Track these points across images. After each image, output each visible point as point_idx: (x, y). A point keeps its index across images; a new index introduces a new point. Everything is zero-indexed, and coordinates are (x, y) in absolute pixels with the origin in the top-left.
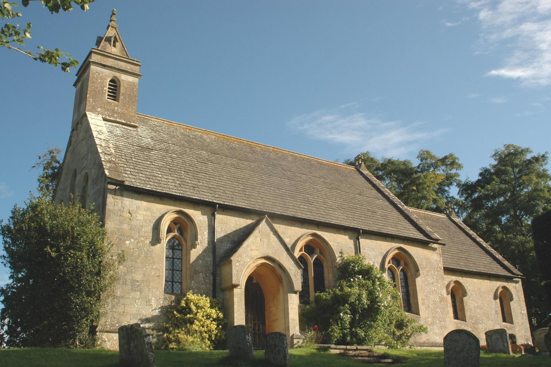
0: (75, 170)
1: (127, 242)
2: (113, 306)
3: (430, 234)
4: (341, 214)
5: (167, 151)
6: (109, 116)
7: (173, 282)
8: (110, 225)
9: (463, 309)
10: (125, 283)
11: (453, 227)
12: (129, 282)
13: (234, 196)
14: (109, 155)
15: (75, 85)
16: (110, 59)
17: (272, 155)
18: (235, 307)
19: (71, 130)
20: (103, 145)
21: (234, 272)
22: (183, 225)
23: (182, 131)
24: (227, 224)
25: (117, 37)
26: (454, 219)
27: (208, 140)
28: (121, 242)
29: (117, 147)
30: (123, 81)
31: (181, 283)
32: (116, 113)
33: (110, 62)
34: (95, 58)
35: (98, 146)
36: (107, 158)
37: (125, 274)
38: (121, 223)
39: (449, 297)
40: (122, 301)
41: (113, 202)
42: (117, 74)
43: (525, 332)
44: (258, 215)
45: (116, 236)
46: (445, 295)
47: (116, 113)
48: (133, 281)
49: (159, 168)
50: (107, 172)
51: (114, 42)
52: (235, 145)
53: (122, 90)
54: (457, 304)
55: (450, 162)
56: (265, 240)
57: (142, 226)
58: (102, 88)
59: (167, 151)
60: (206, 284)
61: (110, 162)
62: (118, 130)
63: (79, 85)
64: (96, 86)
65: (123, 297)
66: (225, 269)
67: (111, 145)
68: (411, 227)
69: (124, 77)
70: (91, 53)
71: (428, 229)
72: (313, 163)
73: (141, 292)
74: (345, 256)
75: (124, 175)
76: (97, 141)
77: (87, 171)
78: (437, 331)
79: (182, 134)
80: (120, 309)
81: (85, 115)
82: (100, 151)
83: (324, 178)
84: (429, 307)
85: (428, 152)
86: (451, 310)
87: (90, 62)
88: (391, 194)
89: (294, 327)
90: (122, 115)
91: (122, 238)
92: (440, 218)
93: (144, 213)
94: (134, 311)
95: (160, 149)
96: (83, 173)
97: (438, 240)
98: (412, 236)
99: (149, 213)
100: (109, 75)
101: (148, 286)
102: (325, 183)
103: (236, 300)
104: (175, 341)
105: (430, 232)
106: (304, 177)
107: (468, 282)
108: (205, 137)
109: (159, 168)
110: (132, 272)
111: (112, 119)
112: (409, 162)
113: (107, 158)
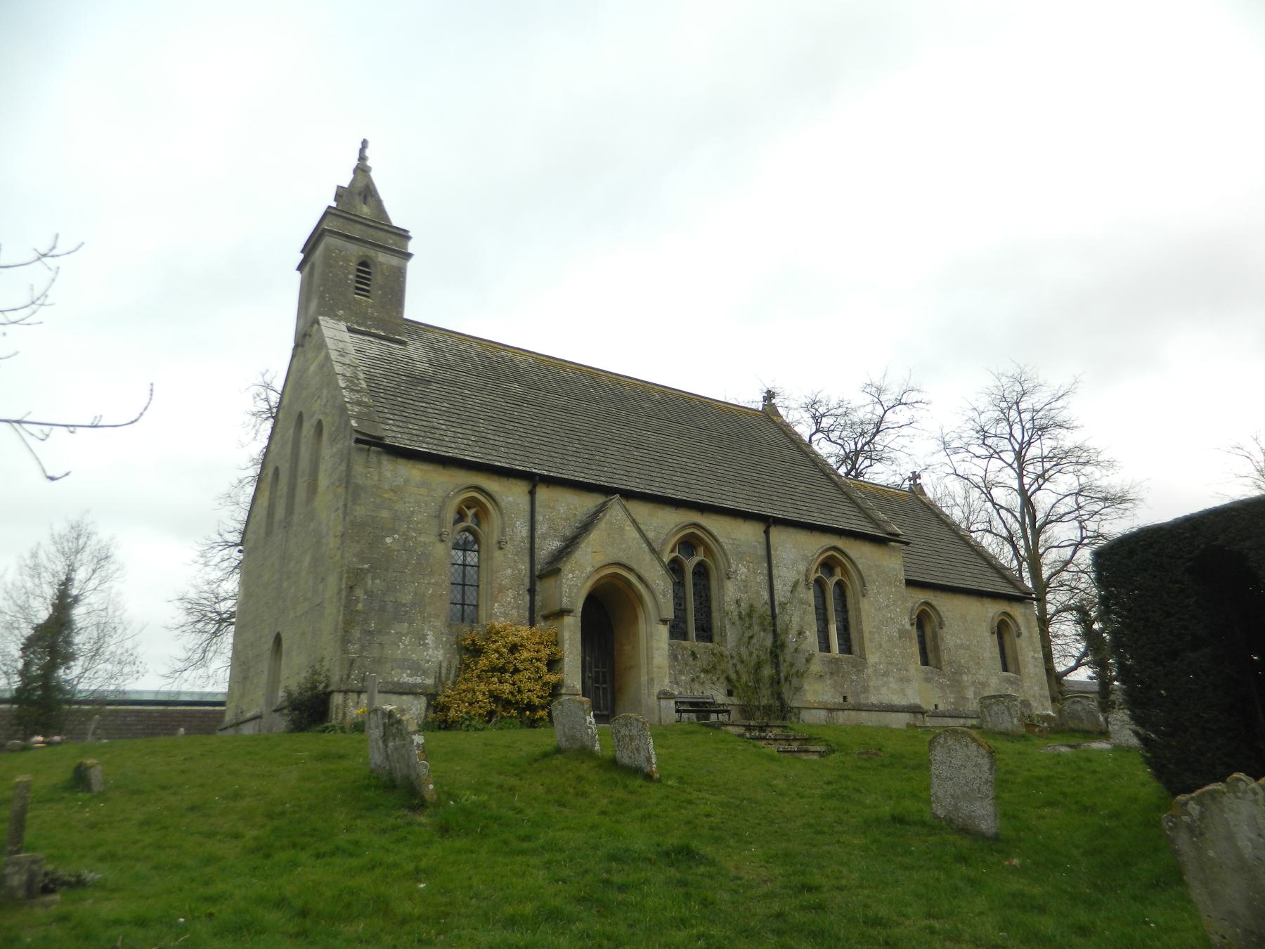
1: (388, 540)
3: (884, 524)
6: (359, 324)
9: (936, 648)
14: (357, 391)
15: (300, 268)
19: (292, 345)
24: (564, 508)
30: (381, 264)
31: (477, 606)
32: (371, 318)
39: (914, 631)
42: (371, 252)
43: (1041, 688)
44: (607, 491)
46: (908, 627)
47: (371, 318)
50: (1242, 775)
54: (928, 640)
57: (413, 512)
58: (346, 275)
60: (518, 608)
61: (359, 403)
62: (374, 348)
63: (307, 269)
65: (379, 632)
67: (362, 376)
73: (410, 623)
78: (893, 686)
79: (479, 354)
84: (881, 646)
86: (916, 649)
96: (314, 421)
97: (898, 535)
98: (853, 528)
107: (947, 606)
113: (356, 396)
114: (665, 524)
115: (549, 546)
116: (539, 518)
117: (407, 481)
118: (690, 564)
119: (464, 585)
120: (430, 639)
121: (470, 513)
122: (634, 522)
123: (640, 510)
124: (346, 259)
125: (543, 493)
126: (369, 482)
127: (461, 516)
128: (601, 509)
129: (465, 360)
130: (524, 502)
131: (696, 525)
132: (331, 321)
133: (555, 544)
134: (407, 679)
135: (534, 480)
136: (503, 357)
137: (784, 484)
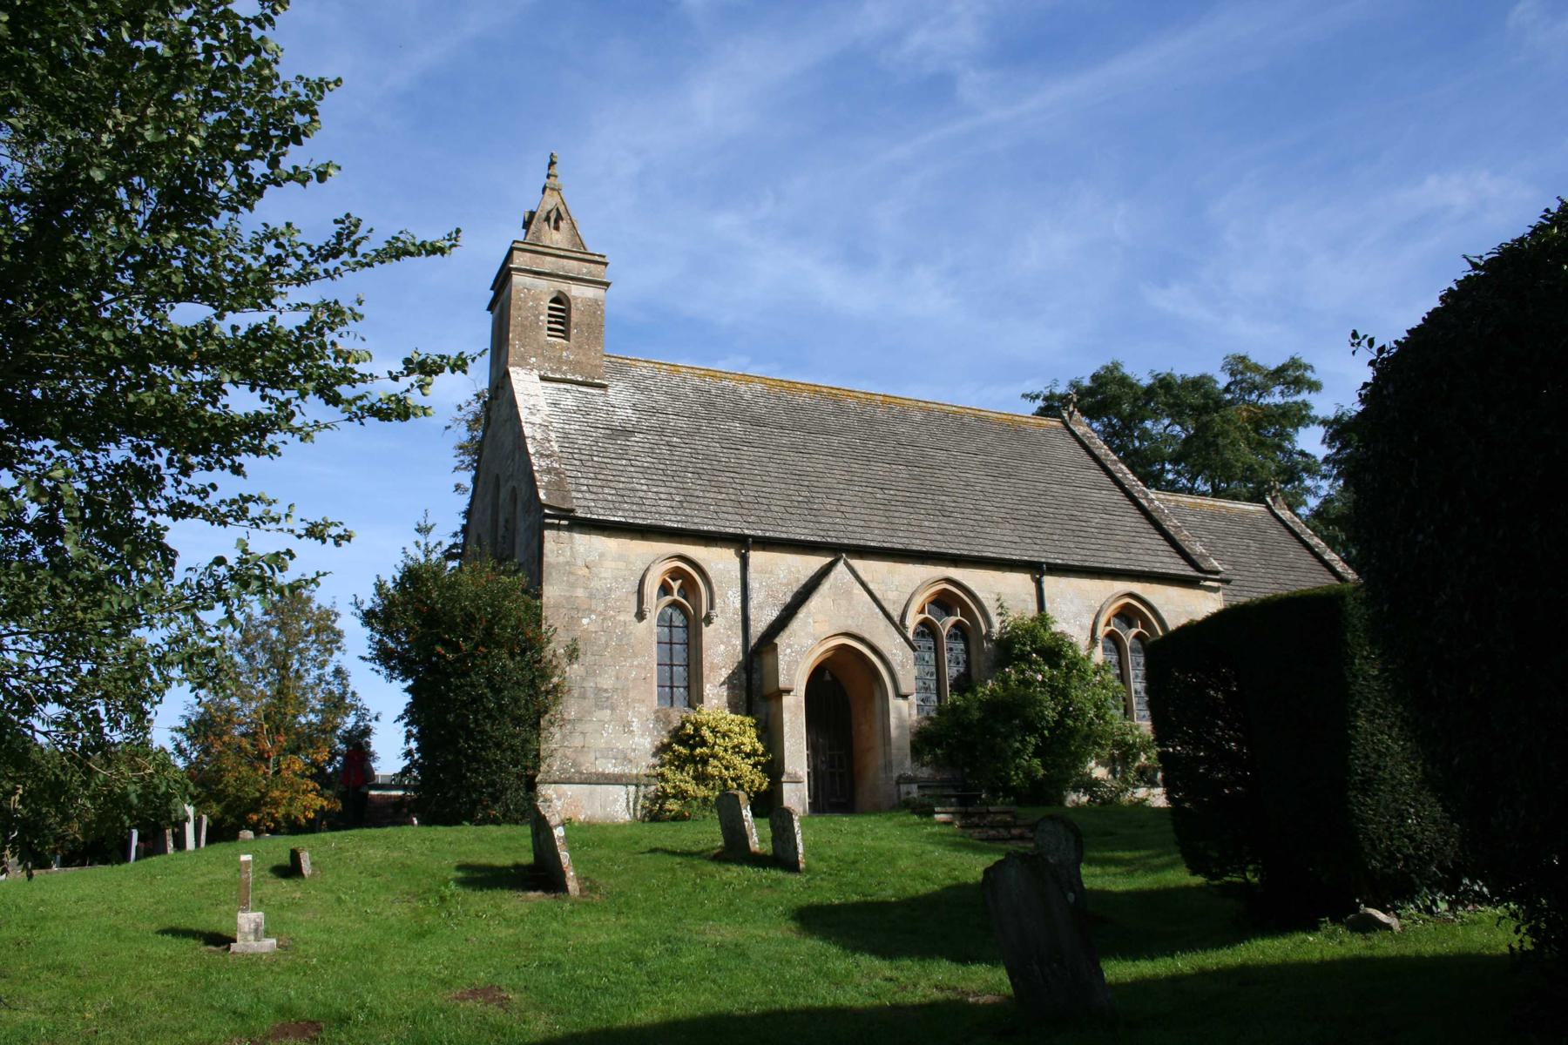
0: (497, 477)
1: (585, 621)
2: (564, 737)
4: (1007, 532)
5: (661, 432)
6: (552, 370)
7: (671, 687)
8: (552, 592)
10: (583, 696)
11: (1275, 532)
12: (590, 694)
13: (787, 516)
14: (548, 456)
15: (490, 308)
16: (548, 258)
17: (880, 414)
18: (786, 729)
20: (538, 437)
21: (782, 666)
22: (687, 586)
23: (697, 381)
24: (779, 572)
25: (562, 209)
26: (1279, 512)
27: (748, 396)
28: (574, 621)
29: (565, 436)
30: (576, 298)
32: (566, 362)
33: (548, 264)
34: (520, 260)
35: (529, 441)
36: (544, 463)
37: (583, 679)
38: (572, 586)
40: (579, 728)
41: (559, 547)
42: (564, 286)
44: (837, 551)
45: (564, 611)
47: (566, 362)
48: (599, 690)
49: (644, 471)
50: (542, 495)
51: (556, 222)
52: (803, 399)
53: (575, 317)
55: (1292, 375)
56: (843, 602)
57: (610, 589)
58: (537, 317)
59: (661, 432)
61: (549, 471)
62: (570, 398)
64: (524, 314)
65: (580, 720)
66: (768, 659)
67: (553, 435)
68: (1164, 546)
69: (576, 291)
70: (512, 250)
71: (1198, 548)
72: (966, 420)
73: (613, 709)
74: (1013, 614)
75: (574, 494)
76: (527, 430)
77: (515, 484)
79: (696, 389)
80: (577, 741)
81: (507, 374)
82: (531, 450)
83: (987, 454)
85: (1243, 359)
87: (511, 269)
88: (1131, 476)
89: (902, 763)
90: (576, 366)
91: (574, 613)
92: (1249, 512)
93: (613, 565)
94: (602, 743)
95: (650, 429)
97: (1217, 573)
98: (1159, 568)
99: (622, 565)
100: (547, 287)
101: (625, 698)
102: (986, 464)
103: (786, 716)
104: (675, 796)
105: (1201, 555)
106: (942, 455)
108: (743, 388)
109: (644, 471)
110: (595, 675)
111: (558, 376)
112: (1210, 379)
113: (544, 463)
114: (907, 584)
115: (761, 620)
116: (753, 584)
117: (601, 555)
118: (946, 624)
119: (672, 665)
120: (636, 726)
121: (676, 585)
122: (863, 584)
123: (869, 568)
124: (536, 299)
125: (757, 557)
126: (561, 559)
127: (665, 589)
128: (824, 572)
129: (676, 398)
130: (736, 563)
131: (949, 580)
132: (522, 372)
133: (771, 614)
134: (611, 768)
135: (742, 544)
136: (723, 389)
137: (1072, 517)
